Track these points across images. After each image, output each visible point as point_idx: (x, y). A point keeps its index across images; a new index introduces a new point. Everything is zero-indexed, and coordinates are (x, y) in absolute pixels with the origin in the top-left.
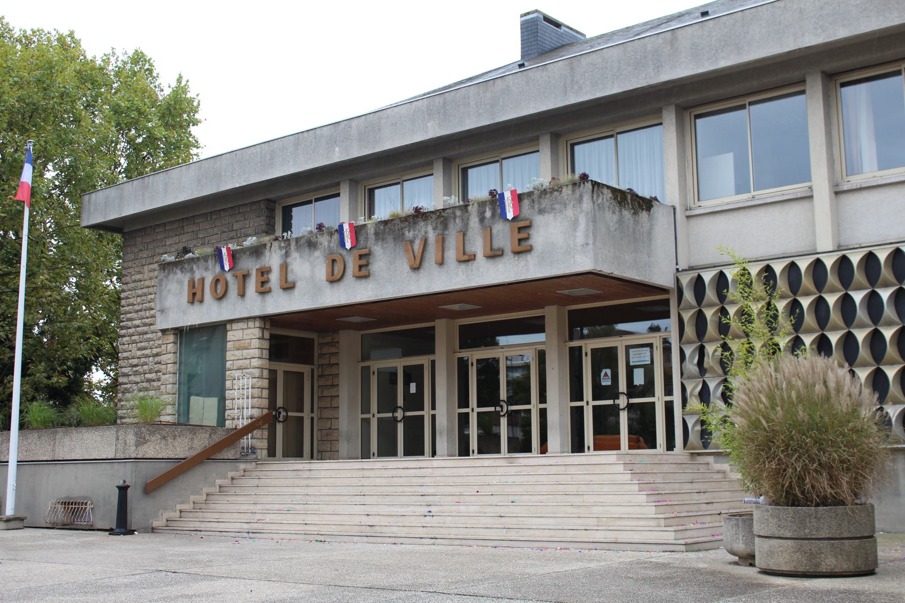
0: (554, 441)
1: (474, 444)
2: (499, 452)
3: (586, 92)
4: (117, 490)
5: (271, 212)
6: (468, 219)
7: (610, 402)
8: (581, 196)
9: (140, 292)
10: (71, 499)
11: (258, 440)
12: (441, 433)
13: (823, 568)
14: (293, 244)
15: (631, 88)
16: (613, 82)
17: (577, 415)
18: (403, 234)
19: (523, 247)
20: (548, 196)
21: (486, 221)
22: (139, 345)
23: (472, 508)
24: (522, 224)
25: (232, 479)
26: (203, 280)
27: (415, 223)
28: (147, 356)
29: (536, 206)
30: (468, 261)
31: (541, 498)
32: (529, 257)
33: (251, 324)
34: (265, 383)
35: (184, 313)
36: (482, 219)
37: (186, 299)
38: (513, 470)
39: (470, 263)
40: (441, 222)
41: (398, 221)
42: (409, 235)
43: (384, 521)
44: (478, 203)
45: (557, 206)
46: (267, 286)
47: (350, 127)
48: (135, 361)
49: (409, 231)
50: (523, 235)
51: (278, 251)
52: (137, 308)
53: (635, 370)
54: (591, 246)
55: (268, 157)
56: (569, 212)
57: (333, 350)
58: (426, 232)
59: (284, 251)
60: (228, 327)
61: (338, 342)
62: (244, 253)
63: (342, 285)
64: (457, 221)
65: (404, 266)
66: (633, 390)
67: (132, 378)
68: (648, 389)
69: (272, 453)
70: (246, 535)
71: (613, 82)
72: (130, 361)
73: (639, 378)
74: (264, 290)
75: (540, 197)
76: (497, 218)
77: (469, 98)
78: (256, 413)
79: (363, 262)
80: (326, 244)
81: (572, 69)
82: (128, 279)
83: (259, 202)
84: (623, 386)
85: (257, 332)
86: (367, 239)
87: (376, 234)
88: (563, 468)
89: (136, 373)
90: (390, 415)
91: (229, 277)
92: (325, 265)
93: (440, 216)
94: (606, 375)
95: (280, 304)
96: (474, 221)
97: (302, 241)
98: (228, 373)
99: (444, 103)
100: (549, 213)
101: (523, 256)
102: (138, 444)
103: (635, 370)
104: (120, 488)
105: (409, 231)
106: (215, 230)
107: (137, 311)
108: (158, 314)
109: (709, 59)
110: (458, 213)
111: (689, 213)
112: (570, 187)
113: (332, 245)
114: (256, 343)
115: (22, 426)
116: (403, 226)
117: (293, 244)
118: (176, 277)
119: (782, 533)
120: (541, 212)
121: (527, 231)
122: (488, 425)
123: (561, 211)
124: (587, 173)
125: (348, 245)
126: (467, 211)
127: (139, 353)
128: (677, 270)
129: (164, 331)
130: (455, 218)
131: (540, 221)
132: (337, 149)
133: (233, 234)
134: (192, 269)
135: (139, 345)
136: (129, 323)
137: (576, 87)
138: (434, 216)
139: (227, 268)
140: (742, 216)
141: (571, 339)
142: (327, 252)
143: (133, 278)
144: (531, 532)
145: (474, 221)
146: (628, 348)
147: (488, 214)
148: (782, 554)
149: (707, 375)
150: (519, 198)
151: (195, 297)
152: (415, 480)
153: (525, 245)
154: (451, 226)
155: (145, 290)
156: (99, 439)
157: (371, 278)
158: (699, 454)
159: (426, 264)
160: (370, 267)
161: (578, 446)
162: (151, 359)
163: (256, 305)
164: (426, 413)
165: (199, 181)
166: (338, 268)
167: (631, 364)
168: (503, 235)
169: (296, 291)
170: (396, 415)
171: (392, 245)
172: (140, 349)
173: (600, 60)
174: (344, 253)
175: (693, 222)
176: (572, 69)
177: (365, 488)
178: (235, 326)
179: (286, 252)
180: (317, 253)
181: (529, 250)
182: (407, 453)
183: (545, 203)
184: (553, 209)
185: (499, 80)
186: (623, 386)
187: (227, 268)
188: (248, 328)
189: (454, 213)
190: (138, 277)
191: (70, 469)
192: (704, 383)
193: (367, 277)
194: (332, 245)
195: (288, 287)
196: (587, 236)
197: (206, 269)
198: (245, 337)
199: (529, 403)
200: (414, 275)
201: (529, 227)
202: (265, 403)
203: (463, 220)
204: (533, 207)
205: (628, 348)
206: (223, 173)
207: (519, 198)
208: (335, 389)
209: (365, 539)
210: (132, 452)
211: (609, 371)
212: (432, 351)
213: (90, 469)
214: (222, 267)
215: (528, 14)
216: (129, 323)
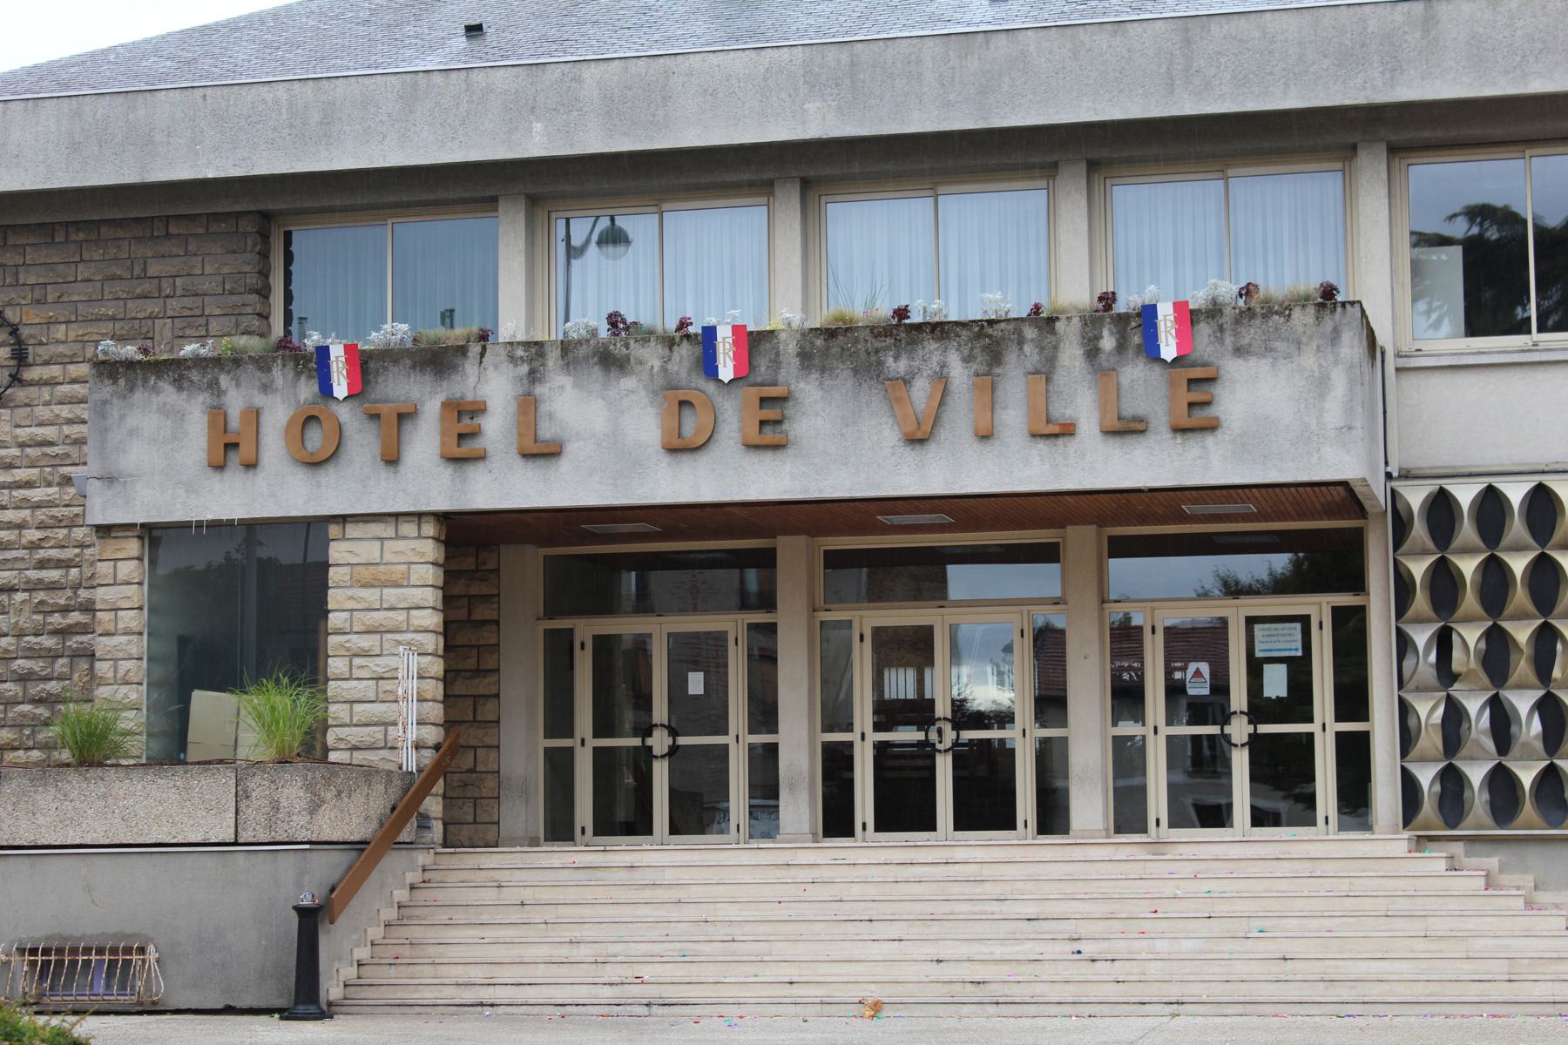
0: (1089, 803)
3: (1222, 96)
4: (294, 914)
5: (265, 237)
6: (1055, 348)
7: (1264, 729)
8: (1336, 332)
10: (66, 939)
12: (792, 787)
14: (553, 357)
15: (1328, 104)
16: (1287, 85)
18: (880, 363)
19: (1196, 422)
20: (1258, 322)
21: (1103, 357)
23: (1186, 945)
24: (1197, 373)
25: (412, 888)
26: (254, 416)
27: (913, 343)
29: (1229, 340)
30: (1056, 436)
31: (1328, 923)
32: (1210, 440)
33: (408, 529)
35: (190, 488)
36: (1092, 353)
37: (203, 456)
38: (1160, 869)
39: (1060, 441)
40: (984, 348)
41: (866, 334)
42: (897, 365)
43: (1001, 972)
44: (1083, 318)
45: (1278, 345)
47: (578, 80)
49: (896, 358)
50: (1197, 396)
51: (507, 368)
53: (1267, 668)
55: (316, 117)
56: (1309, 360)
57: (485, 589)
58: (943, 366)
59: (524, 369)
60: (334, 530)
61: (497, 571)
62: (396, 362)
63: (703, 461)
64: (1027, 348)
65: (890, 435)
66: (1260, 709)
68: (1298, 703)
70: (644, 1010)
71: (1287, 85)
73: (1276, 683)
74: (463, 450)
75: (1238, 321)
76: (1130, 353)
77: (919, 62)
79: (770, 413)
81: (1188, 42)
83: (237, 215)
84: (1239, 698)
85: (431, 550)
86: (776, 363)
87: (805, 356)
88: (1308, 865)
91: (345, 413)
92: (652, 411)
93: (980, 335)
94: (1198, 673)
97: (583, 351)
99: (853, 64)
100: (1262, 356)
102: (314, 808)
103: (1267, 668)
104: (302, 912)
105: (896, 358)
106: (83, 270)
108: (94, 487)
109: (1507, 72)
110: (1030, 333)
111: (1403, 363)
112: (1311, 310)
113: (673, 367)
116: (877, 344)
117: (553, 357)
118: (162, 398)
120: (1239, 351)
121: (1205, 387)
123: (1288, 356)
124: (1334, 282)
125: (726, 372)
126: (1053, 332)
128: (1389, 476)
129: (105, 531)
130: (1021, 342)
131: (1235, 370)
132: (538, 126)
133: (147, 286)
134: (213, 386)
137: (1196, 81)
138: (964, 333)
140: (1516, 379)
142: (659, 381)
144: (1386, 986)
145: (1071, 355)
146: (1251, 621)
147: (1108, 342)
149: (1456, 686)
150: (1188, 317)
151: (231, 450)
152: (956, 889)
153: (1200, 415)
154: (1011, 357)
156: (173, 795)
157: (790, 451)
158: (1431, 839)
159: (943, 434)
160: (786, 426)
161: (837, 821)
163: (426, 483)
165: (75, 147)
167: (1259, 654)
169: (565, 464)
170: (649, 742)
171: (849, 383)
173: (1256, 34)
174: (711, 387)
175: (1409, 380)
176: (1188, 42)
177: (846, 906)
179: (532, 372)
180: (628, 383)
181: (1211, 427)
183: (1251, 334)
184: (1269, 350)
185: (1003, 36)
186: (1239, 698)
187: (340, 389)
188: (398, 537)
189: (1019, 332)
191: (57, 868)
192: (1449, 699)
194: (673, 367)
196: (1349, 411)
197: (266, 388)
198: (388, 557)
200: (910, 455)
201: (1211, 380)
203: (1042, 349)
204: (1221, 341)
205: (1251, 621)
206: (158, 138)
207: (1188, 317)
208: (492, 678)
209: (992, 1009)
211: (1205, 668)
213: (141, 869)
214: (326, 389)
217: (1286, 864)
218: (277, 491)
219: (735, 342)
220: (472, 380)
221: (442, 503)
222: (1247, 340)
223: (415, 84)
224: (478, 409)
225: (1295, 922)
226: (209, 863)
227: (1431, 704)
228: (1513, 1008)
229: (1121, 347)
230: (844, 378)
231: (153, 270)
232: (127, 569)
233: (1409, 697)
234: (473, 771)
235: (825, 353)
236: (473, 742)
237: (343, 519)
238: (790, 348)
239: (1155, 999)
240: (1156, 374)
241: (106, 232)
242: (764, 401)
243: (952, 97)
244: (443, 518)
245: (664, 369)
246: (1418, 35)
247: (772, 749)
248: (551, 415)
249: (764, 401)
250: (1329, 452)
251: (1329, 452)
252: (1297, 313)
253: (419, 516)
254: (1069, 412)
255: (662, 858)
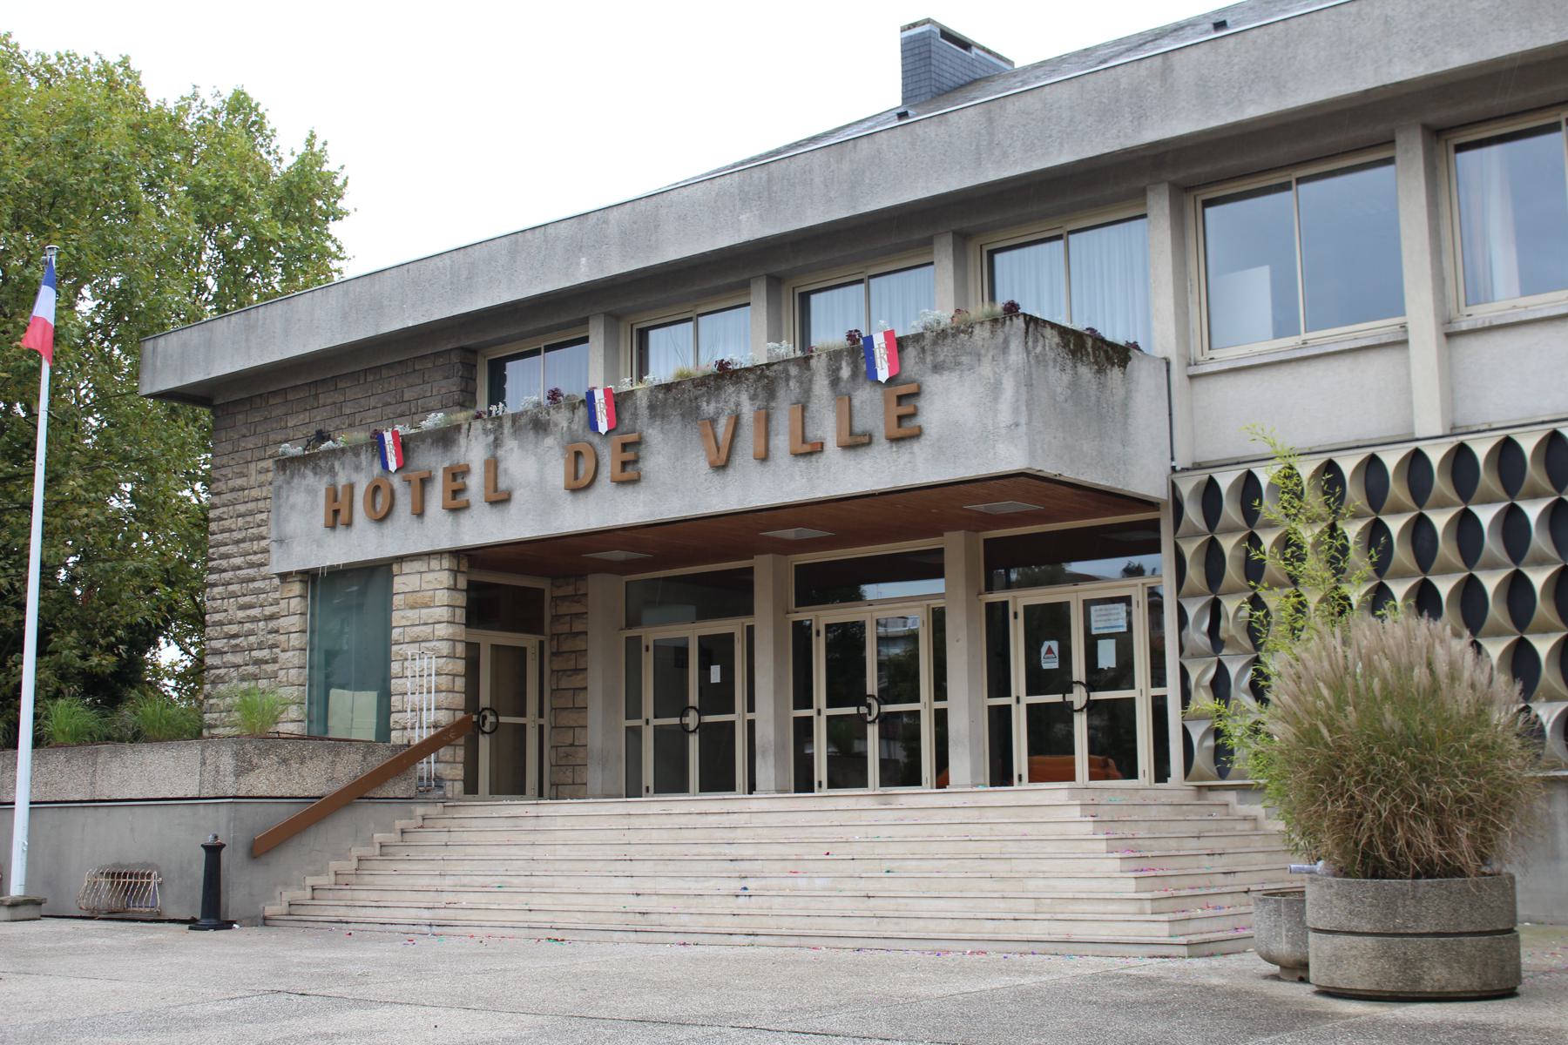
1: (821, 771)
2: (864, 784)
6: (810, 381)
8: (1006, 342)
9: (242, 508)
11: (446, 765)
12: (764, 753)
13: (1427, 986)
14: (507, 425)
17: (1000, 721)
18: (698, 408)
19: (905, 431)
20: (949, 341)
21: (842, 384)
22: (241, 600)
23: (818, 883)
24: (903, 390)
26: (351, 487)
27: (718, 388)
28: (255, 620)
29: (929, 359)
30: (810, 453)
32: (916, 446)
33: (435, 564)
34: (460, 666)
36: (835, 382)
38: (889, 816)
39: (814, 458)
42: (709, 409)
43: (666, 905)
45: (964, 359)
46: (462, 498)
47: (606, 222)
48: (234, 629)
50: (905, 410)
51: (482, 437)
52: (237, 535)
54: (1023, 429)
55: (464, 274)
56: (986, 369)
57: (576, 609)
58: (738, 405)
59: (491, 437)
60: (395, 568)
62: (423, 441)
64: (792, 384)
66: (1096, 678)
67: (229, 658)
68: (1123, 675)
69: (471, 787)
71: (1061, 144)
72: (226, 628)
73: (1107, 657)
74: (457, 504)
75: (935, 343)
76: (861, 380)
77: (811, 171)
78: (444, 718)
79: (629, 456)
80: (565, 424)
81: (990, 121)
82: (221, 486)
83: (449, 351)
84: (1079, 671)
85: (445, 578)
86: (635, 415)
88: (976, 812)
89: (236, 650)
90: (676, 721)
91: (396, 482)
92: (562, 461)
93: (762, 377)
94: (1050, 651)
95: (485, 528)
96: (821, 386)
97: (524, 420)
98: (394, 648)
99: (769, 181)
100: (951, 370)
101: (906, 447)
102: (239, 773)
104: (207, 848)
106: (373, 402)
107: (237, 542)
108: (274, 547)
109: (1227, 104)
110: (794, 371)
111: (1193, 370)
112: (988, 326)
113: (575, 427)
114: (443, 596)
115: (37, 742)
117: (507, 425)
118: (305, 482)
119: (1354, 924)
120: (937, 368)
121: (913, 401)
122: (846, 741)
123: (971, 368)
125: (603, 427)
126: (808, 368)
127: (241, 614)
128: (1173, 468)
130: (787, 380)
131: (934, 384)
132: (583, 260)
133: (403, 407)
135: (241, 600)
136: (224, 563)
137: (997, 152)
138: (752, 377)
139: (393, 466)
141: (990, 588)
142: (567, 438)
143: (231, 484)
145: (821, 386)
146: (1088, 604)
147: (845, 372)
148: (1356, 961)
149: (1225, 651)
150: (898, 345)
151: (338, 518)
152: (719, 834)
153: (909, 425)
154: (781, 393)
155: (251, 506)
156: (171, 763)
157: (643, 484)
158: (1211, 788)
159: (738, 460)
160: (641, 465)
161: (1001, 774)
162: (261, 624)
163: (442, 530)
164: (739, 717)
165: (345, 316)
166: (586, 467)
167: (1094, 632)
168: (871, 408)
169: (513, 507)
171: (679, 427)
172: (242, 607)
175: (1201, 385)
176: (990, 121)
178: (407, 567)
179: (496, 439)
180: (549, 441)
181: (917, 435)
182: (705, 787)
183: (944, 353)
185: (865, 140)
186: (1079, 671)
187: (393, 466)
189: (786, 371)
190: (239, 482)
192: (1220, 665)
193: (634, 481)
194: (575, 427)
195: (499, 499)
196: (1016, 411)
197: (357, 468)
198: (424, 586)
199: (917, 700)
200: (716, 479)
201: (916, 395)
202: (459, 700)
204: (923, 360)
205: (1088, 604)
206: (386, 303)
207: (898, 345)
209: (633, 936)
210: (229, 786)
211: (1054, 645)
212: (749, 611)
214: (385, 465)
215: (914, 25)
216: (224, 563)
217: (960, 812)
218: (361, 543)
219: (607, 402)
220: (463, 449)
221: (446, 544)
222: (942, 358)
223: (516, 242)
224: (465, 471)
225: (914, 863)
226: (185, 811)
227: (1201, 668)
228: (1134, 949)
229: (854, 375)
230: (676, 423)
231: (408, 395)
232: (295, 604)
233: (1186, 664)
234: (572, 745)
235: (664, 404)
236: (572, 723)
237: (401, 559)
238: (643, 402)
239: (738, 931)
240: (878, 394)
241: (385, 373)
242: (625, 447)
243: (832, 194)
244: (457, 554)
245: (569, 428)
246: (1158, 84)
247: (944, 711)
248: (506, 471)
249: (625, 447)
250: (1002, 448)
251: (1002, 448)
252: (977, 330)
253: (439, 554)
254: (819, 433)
255: (695, 810)
